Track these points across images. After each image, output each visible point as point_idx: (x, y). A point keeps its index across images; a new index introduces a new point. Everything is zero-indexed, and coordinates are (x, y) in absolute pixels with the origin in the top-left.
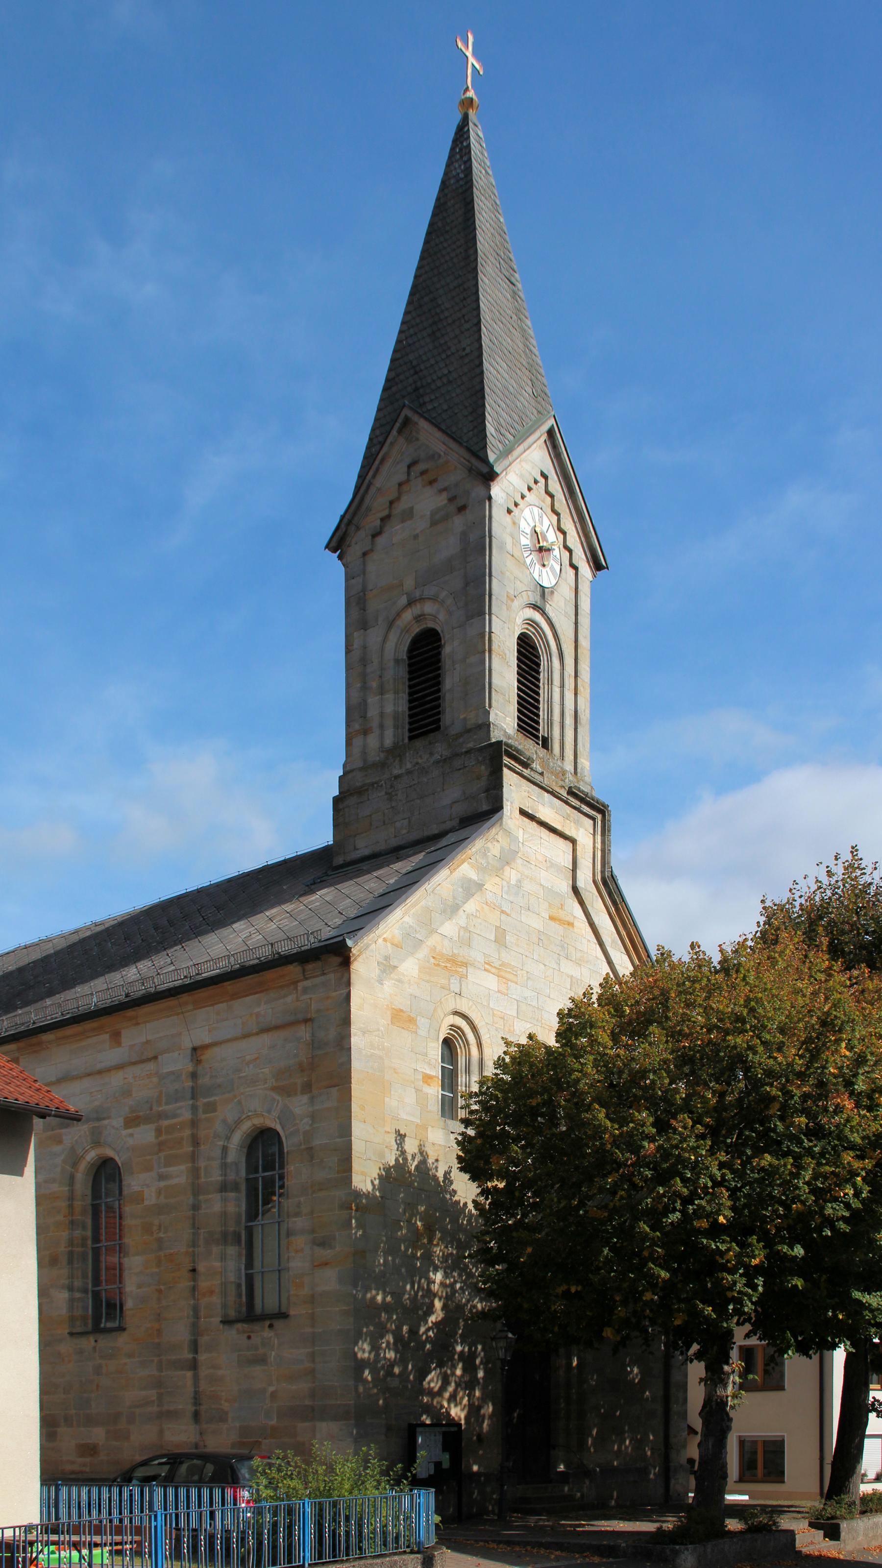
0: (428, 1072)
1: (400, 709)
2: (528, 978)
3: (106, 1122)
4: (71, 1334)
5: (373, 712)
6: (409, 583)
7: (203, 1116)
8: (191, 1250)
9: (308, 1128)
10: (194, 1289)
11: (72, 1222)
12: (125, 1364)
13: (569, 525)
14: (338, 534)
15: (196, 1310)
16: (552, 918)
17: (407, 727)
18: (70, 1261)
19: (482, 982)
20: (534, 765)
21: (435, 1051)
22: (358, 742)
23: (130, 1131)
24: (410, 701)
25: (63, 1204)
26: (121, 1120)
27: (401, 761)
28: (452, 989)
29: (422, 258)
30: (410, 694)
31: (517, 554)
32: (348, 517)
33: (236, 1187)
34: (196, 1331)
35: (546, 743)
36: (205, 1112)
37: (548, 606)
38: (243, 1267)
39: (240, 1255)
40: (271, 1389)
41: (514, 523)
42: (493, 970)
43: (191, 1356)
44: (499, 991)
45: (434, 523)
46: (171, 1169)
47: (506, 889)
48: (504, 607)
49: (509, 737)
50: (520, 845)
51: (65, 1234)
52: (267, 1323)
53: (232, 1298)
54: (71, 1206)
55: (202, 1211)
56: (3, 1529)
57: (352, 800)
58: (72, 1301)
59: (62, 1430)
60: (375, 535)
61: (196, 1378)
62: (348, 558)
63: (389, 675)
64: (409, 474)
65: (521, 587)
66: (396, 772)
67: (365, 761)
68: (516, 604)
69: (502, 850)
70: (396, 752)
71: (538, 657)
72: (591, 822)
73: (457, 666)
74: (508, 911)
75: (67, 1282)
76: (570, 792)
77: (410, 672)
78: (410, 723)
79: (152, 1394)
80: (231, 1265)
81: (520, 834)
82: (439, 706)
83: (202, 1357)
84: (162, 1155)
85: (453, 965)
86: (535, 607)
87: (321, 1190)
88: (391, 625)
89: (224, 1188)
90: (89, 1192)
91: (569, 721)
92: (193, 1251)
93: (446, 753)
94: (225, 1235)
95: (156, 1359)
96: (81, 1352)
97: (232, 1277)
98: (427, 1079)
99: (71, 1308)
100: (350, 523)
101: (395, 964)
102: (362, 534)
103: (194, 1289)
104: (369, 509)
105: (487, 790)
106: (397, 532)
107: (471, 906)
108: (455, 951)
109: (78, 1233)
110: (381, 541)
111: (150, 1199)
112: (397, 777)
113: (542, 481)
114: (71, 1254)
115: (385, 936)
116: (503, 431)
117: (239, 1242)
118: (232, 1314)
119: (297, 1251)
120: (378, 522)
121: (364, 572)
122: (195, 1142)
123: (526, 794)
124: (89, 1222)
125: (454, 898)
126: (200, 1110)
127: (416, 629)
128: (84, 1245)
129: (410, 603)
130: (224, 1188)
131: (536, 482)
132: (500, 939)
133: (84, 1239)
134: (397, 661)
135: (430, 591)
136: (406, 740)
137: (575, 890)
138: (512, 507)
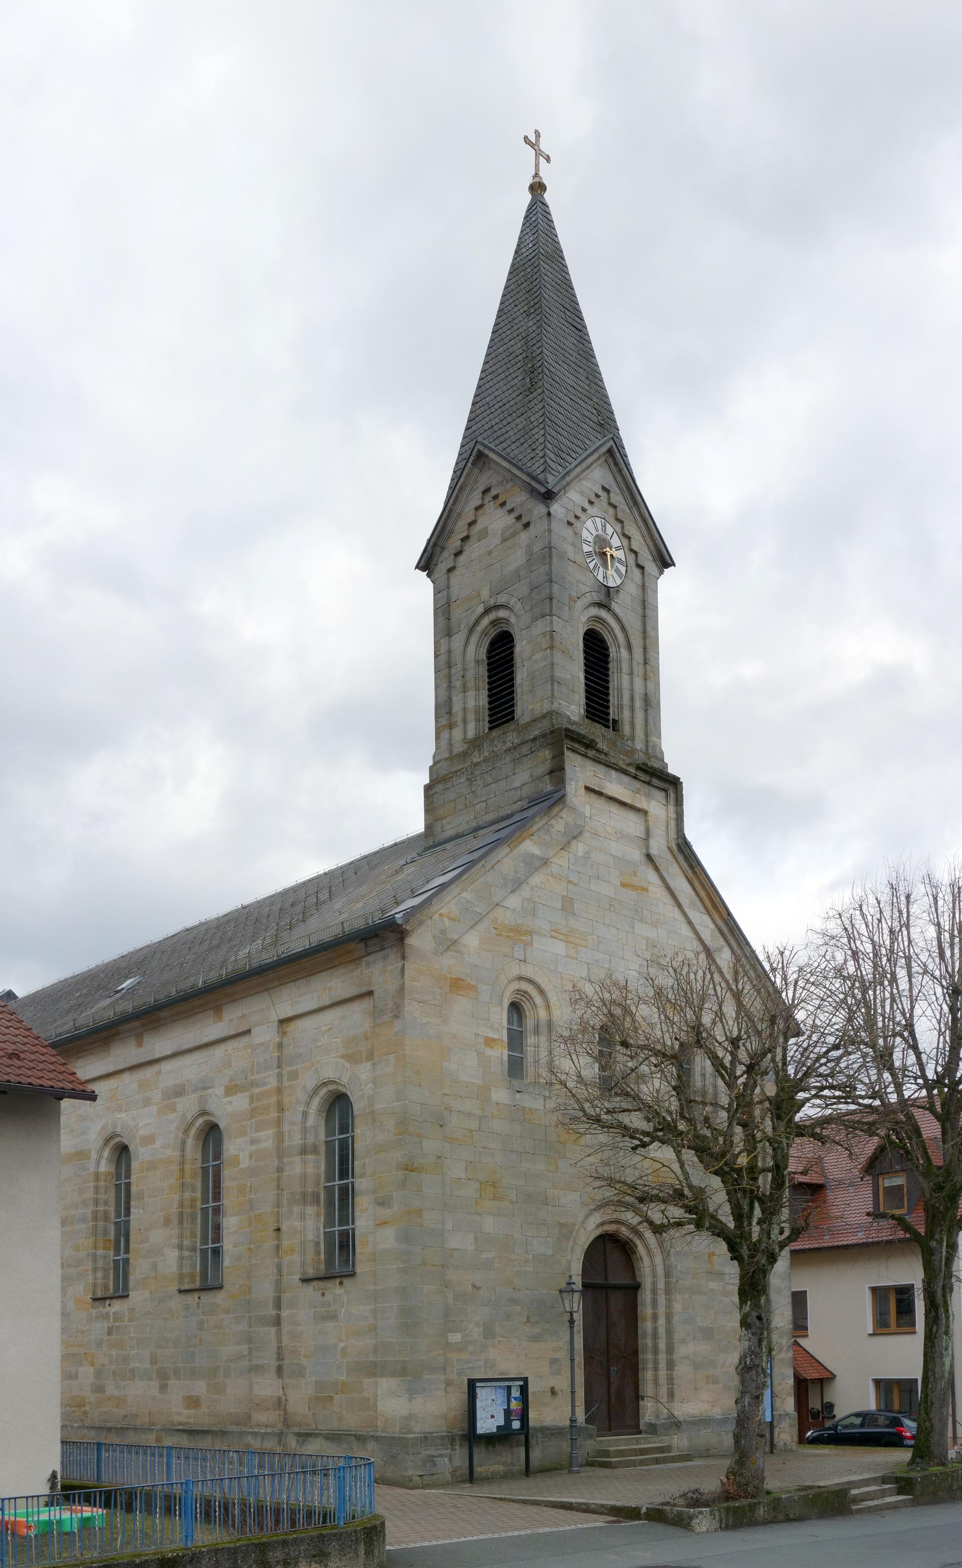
0: (491, 1035)
1: (481, 704)
2: (599, 942)
3: (210, 1091)
4: (180, 1291)
5: (457, 708)
6: (485, 593)
7: (287, 1084)
8: (276, 1210)
9: (371, 1092)
10: (278, 1247)
11: (183, 1185)
12: (223, 1320)
13: (632, 530)
14: (426, 555)
15: (279, 1268)
16: (623, 885)
17: (487, 719)
18: (181, 1222)
19: (549, 948)
20: (600, 746)
21: (500, 1016)
22: (445, 735)
23: (229, 1099)
24: (490, 696)
25: (175, 1168)
26: (222, 1089)
27: (479, 750)
28: (516, 956)
29: (498, 317)
30: (489, 690)
31: (579, 559)
32: (433, 540)
33: (315, 1150)
34: (279, 1287)
35: (616, 725)
36: (289, 1080)
37: (613, 603)
38: (322, 1226)
39: (318, 1214)
40: (342, 1345)
41: (576, 534)
42: (561, 937)
43: (274, 1312)
44: (567, 956)
45: (505, 540)
46: (260, 1134)
47: (572, 860)
48: (566, 608)
49: (575, 723)
50: (587, 819)
51: (176, 1197)
52: (338, 1280)
53: (310, 1256)
54: (182, 1170)
55: (285, 1173)
56: (3, 1500)
57: (440, 787)
58: (181, 1258)
59: (172, 1382)
60: (458, 554)
61: (279, 1332)
62: (436, 575)
63: (470, 674)
64: (483, 499)
65: (584, 589)
66: (475, 760)
67: (451, 752)
68: (580, 604)
69: (567, 825)
70: (475, 744)
71: (607, 649)
72: (663, 794)
73: (525, 663)
74: (576, 882)
75: (177, 1241)
76: (638, 768)
77: (489, 671)
78: (490, 716)
79: (244, 1348)
80: (310, 1224)
81: (587, 811)
82: (513, 699)
83: (285, 1313)
84: (253, 1120)
85: (519, 934)
86: (600, 605)
87: (381, 1152)
88: (471, 631)
89: (304, 1151)
90: (199, 1156)
91: (638, 703)
92: (278, 1212)
93: (517, 741)
94: (304, 1195)
95: (247, 1315)
96: (187, 1308)
97: (310, 1236)
98: (490, 1042)
99: (180, 1266)
100: (435, 545)
101: (455, 937)
102: (446, 554)
103: (278, 1247)
104: (452, 532)
105: (551, 772)
106: (474, 550)
107: (536, 879)
108: (519, 921)
109: (187, 1195)
110: (462, 559)
111: (245, 1163)
112: (476, 765)
113: (603, 494)
114: (181, 1214)
115: (441, 911)
116: (563, 455)
117: (318, 1202)
118: (311, 1273)
119: (362, 1211)
120: (459, 543)
121: (448, 588)
122: (281, 1108)
123: (592, 773)
124: (199, 1185)
125: (516, 872)
126: (285, 1079)
127: (493, 633)
128: (193, 1206)
129: (487, 611)
130: (304, 1151)
131: (597, 496)
132: (568, 906)
133: (193, 1200)
134: (477, 662)
135: (502, 599)
136: (487, 731)
137: (649, 857)
138: (573, 520)
